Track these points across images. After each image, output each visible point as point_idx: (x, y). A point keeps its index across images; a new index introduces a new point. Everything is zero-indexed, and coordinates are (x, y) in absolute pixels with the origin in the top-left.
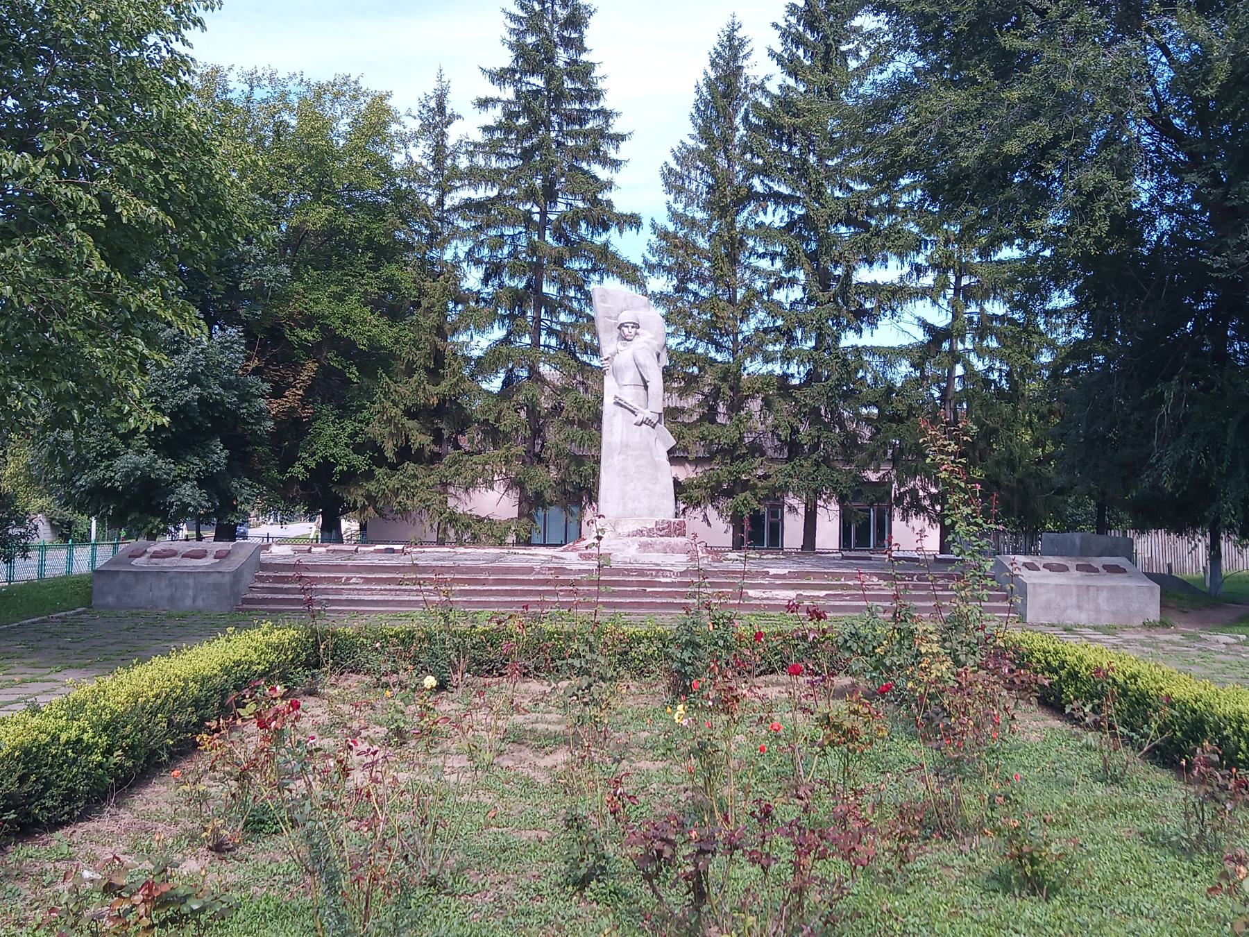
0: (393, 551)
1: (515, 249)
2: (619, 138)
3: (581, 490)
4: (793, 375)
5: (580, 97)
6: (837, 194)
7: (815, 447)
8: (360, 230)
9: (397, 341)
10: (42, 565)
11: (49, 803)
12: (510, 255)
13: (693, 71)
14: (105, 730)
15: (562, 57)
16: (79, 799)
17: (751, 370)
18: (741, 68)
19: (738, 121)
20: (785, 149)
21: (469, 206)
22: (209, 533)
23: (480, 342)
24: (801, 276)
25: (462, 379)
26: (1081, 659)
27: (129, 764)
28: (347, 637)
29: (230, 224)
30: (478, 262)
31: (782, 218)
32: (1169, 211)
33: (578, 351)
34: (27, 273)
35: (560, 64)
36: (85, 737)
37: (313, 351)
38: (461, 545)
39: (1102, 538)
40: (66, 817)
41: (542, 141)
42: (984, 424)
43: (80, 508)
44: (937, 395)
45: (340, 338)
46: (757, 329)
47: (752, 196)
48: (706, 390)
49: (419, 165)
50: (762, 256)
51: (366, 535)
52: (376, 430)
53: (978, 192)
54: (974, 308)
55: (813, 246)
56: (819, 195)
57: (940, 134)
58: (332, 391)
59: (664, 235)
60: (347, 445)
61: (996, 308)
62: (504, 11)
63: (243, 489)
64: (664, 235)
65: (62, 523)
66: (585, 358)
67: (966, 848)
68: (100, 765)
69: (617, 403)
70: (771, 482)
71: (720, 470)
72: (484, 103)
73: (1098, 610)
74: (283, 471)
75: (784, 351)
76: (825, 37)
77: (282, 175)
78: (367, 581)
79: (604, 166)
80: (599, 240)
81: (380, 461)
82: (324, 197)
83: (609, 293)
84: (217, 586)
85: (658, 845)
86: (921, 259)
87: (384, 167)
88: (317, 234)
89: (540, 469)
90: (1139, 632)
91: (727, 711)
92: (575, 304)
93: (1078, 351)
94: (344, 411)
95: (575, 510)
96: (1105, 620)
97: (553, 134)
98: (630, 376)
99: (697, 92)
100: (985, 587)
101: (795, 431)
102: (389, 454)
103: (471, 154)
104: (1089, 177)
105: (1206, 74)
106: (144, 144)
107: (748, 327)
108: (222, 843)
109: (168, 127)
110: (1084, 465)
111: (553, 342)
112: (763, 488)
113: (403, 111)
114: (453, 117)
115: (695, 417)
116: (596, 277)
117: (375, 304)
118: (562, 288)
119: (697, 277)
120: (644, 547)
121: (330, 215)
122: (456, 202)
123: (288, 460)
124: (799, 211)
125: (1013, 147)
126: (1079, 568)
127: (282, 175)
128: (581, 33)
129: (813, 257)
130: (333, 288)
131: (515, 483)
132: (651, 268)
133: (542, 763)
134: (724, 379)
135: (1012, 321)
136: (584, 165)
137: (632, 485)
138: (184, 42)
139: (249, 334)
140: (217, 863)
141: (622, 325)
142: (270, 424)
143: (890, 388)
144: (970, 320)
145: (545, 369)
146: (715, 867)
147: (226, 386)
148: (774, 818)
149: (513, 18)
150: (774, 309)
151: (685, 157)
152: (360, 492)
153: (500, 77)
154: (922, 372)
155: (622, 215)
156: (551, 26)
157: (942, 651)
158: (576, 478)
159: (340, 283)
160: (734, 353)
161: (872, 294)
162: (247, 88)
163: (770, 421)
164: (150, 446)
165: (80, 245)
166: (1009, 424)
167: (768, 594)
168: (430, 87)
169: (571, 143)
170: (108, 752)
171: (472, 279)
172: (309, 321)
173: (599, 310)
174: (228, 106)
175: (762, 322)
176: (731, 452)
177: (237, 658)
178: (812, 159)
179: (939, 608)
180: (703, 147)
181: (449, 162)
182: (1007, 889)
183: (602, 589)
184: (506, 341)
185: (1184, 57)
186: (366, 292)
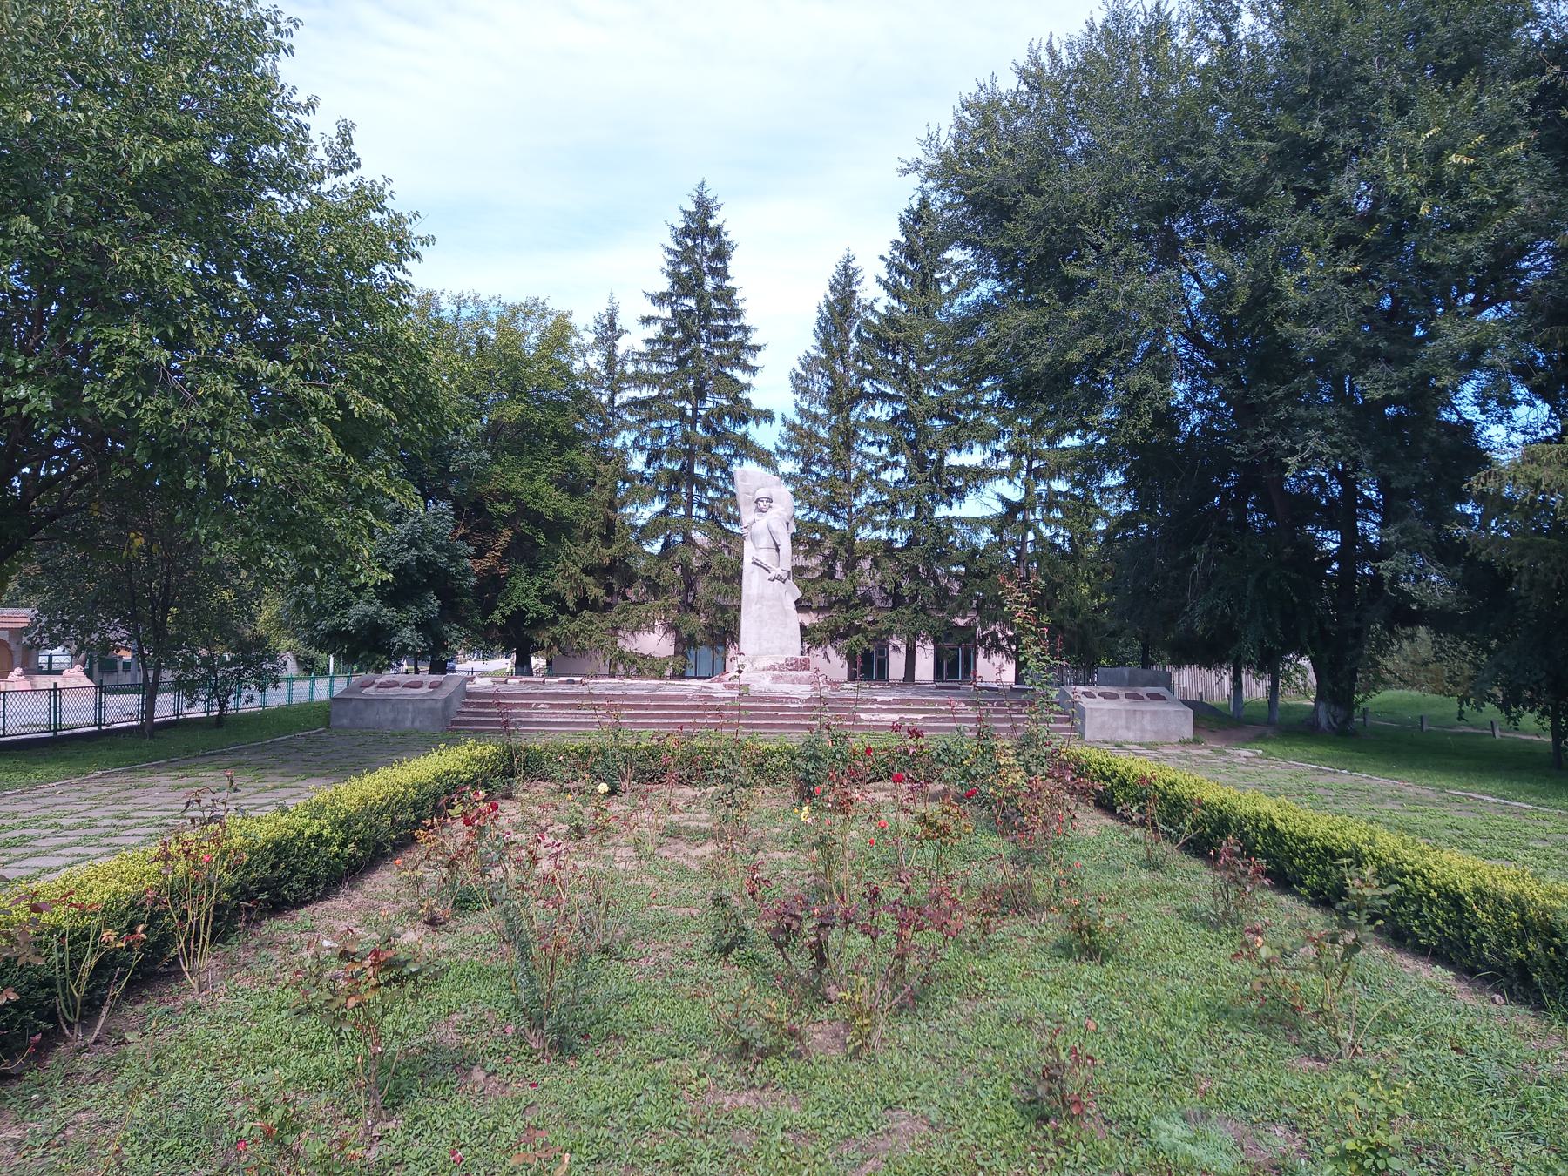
2: (756, 348)
3: (725, 634)
5: (725, 315)
6: (932, 393)
10: (290, 694)
11: (296, 886)
12: (668, 443)
13: (816, 294)
15: (710, 283)
19: (852, 335)
21: (634, 403)
23: (643, 514)
24: (903, 460)
25: (629, 544)
26: (1129, 770)
27: (360, 854)
30: (642, 449)
32: (1200, 407)
33: (723, 521)
35: (709, 289)
37: (509, 520)
39: (1146, 672)
41: (694, 351)
43: (321, 647)
45: (531, 510)
47: (863, 395)
49: (595, 371)
50: (872, 444)
51: (551, 669)
52: (559, 584)
53: (1046, 393)
54: (1042, 486)
55: (913, 436)
57: (1015, 345)
58: (524, 553)
59: (792, 427)
61: (1060, 486)
63: (452, 632)
64: (792, 427)
65: (306, 660)
66: (728, 526)
67: (1036, 922)
68: (337, 855)
70: (878, 626)
71: (838, 617)
72: (647, 321)
73: (1143, 730)
74: (484, 618)
76: (922, 267)
80: (740, 431)
81: (563, 609)
83: (747, 472)
84: (431, 711)
88: (512, 426)
89: (692, 615)
91: (843, 812)
93: (1126, 521)
94: (534, 569)
95: (721, 649)
96: (1148, 738)
98: (765, 541)
100: (1051, 711)
101: (898, 585)
102: (570, 604)
103: (637, 362)
104: (1136, 380)
106: (372, 354)
107: (861, 502)
110: (1121, 619)
111: (703, 513)
113: (581, 327)
114: (622, 332)
115: (818, 574)
116: (738, 461)
117: (560, 483)
118: (710, 470)
120: (776, 679)
122: (625, 400)
123: (489, 609)
124: (901, 408)
125: (1074, 356)
126: (1127, 696)
130: (525, 470)
131: (672, 628)
132: (782, 453)
133: (693, 854)
134: (841, 543)
135: (1073, 497)
136: (728, 371)
138: (405, 271)
139: (457, 507)
140: (431, 934)
142: (474, 580)
143: (975, 551)
144: (1040, 495)
145: (696, 535)
147: (438, 549)
149: (670, 251)
150: (881, 487)
151: (809, 364)
153: (660, 299)
158: (721, 624)
159: (530, 465)
160: (849, 522)
161: (961, 475)
162: (455, 309)
163: (877, 577)
165: (320, 435)
168: (603, 307)
169: (717, 353)
170: (343, 844)
171: (638, 462)
172: (506, 497)
173: (740, 488)
174: (440, 323)
176: (846, 603)
179: (1014, 728)
180: (824, 356)
182: (1070, 955)
184: (664, 512)
185: (1212, 283)
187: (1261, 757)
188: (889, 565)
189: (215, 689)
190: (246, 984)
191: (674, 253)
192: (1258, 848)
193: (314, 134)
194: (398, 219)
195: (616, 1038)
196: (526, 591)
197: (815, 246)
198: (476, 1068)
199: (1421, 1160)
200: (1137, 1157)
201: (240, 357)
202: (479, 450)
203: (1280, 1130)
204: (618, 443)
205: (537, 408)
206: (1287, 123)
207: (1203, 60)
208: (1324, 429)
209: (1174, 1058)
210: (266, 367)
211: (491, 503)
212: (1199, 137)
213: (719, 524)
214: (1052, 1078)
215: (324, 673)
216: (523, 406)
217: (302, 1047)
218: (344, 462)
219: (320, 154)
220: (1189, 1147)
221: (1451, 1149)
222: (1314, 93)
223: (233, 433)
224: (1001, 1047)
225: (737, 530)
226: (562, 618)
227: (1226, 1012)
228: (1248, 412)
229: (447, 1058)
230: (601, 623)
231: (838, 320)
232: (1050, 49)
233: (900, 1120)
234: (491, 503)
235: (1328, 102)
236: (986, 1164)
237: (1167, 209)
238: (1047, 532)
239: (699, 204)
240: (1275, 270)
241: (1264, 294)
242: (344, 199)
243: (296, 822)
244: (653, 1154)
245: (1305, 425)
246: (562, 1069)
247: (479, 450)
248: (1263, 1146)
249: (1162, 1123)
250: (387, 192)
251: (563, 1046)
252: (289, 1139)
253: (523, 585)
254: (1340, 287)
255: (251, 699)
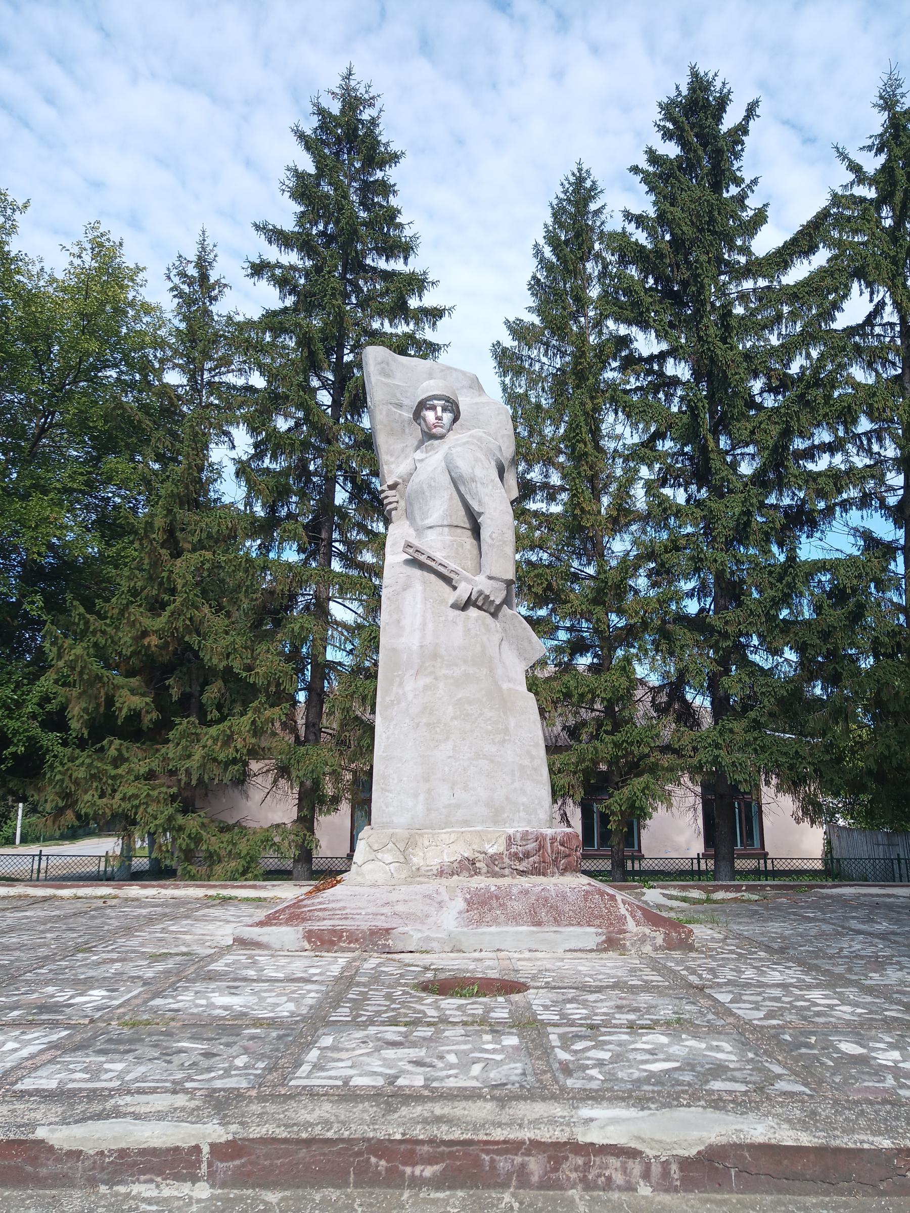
60: (34, 716)
69: (414, 562)
98: (441, 507)
99: (536, 255)
120: (481, 906)
141: (423, 405)
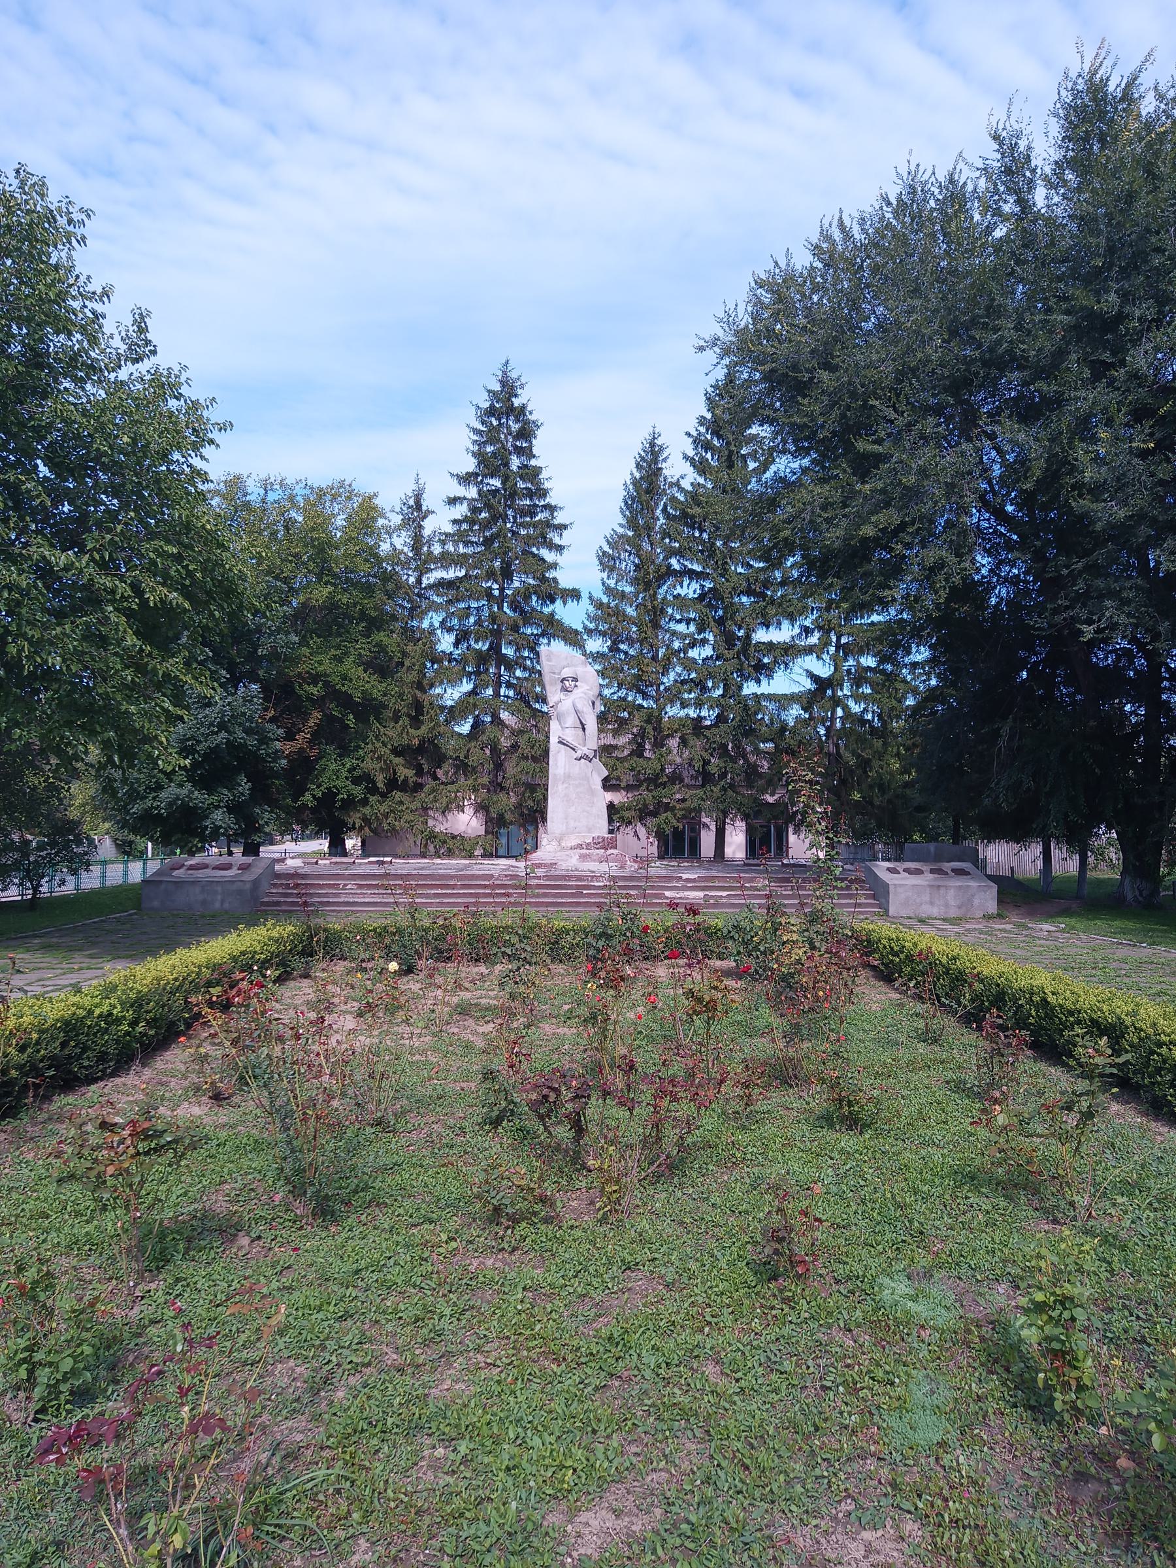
0: (383, 863)
1: (480, 619)
2: (562, 527)
3: (533, 815)
4: (705, 718)
5: (530, 494)
6: (740, 570)
7: (723, 775)
8: (355, 605)
9: (385, 695)
10: (103, 876)
11: (86, 1063)
12: (475, 623)
13: (622, 472)
14: (132, 1006)
15: (515, 462)
16: (111, 1060)
17: (670, 714)
18: (661, 469)
19: (658, 512)
20: (697, 534)
21: (442, 584)
22: (238, 850)
23: (452, 694)
24: (711, 638)
25: (438, 724)
26: (915, 945)
27: (152, 1032)
28: (336, 932)
29: (242, 603)
30: (450, 630)
31: (695, 591)
32: (1005, 580)
33: (531, 702)
34: (74, 646)
35: (514, 468)
36: (115, 1012)
37: (318, 703)
38: (439, 857)
39: (956, 847)
40: (100, 1074)
41: (500, 530)
42: (860, 755)
43: (134, 830)
44: (822, 732)
45: (339, 691)
46: (676, 681)
47: (670, 572)
48: (635, 730)
49: (402, 552)
50: (679, 621)
51: (367, 849)
52: (369, 765)
53: (847, 571)
54: (851, 662)
55: (721, 612)
56: (725, 572)
57: (811, 521)
58: (335, 735)
59: (599, 605)
61: (869, 661)
62: (468, 426)
63: (265, 816)
64: (599, 605)
65: (124, 842)
66: (537, 706)
67: (804, 1094)
68: (128, 1033)
69: (560, 742)
70: (688, 803)
71: (646, 795)
72: (453, 501)
73: (947, 905)
74: (295, 800)
75: (697, 698)
76: (728, 443)
77: (291, 562)
78: (360, 886)
79: (550, 550)
80: (547, 610)
81: (374, 790)
82: (325, 579)
83: (555, 655)
84: (240, 892)
85: (545, 1091)
86: (808, 623)
87: (374, 556)
88: (321, 608)
89: (502, 795)
90: (980, 923)
91: (615, 988)
92: (528, 662)
93: (932, 696)
94: (345, 751)
95: (531, 828)
96: (953, 913)
97: (509, 525)
98: (571, 720)
100: (835, 887)
101: (706, 763)
102: (380, 785)
103: (443, 543)
104: (931, 555)
105: (1026, 472)
106: (168, 542)
107: (669, 679)
108: (219, 1093)
109: (187, 526)
110: (922, 791)
111: (511, 693)
112: (681, 809)
113: (387, 509)
114: (429, 512)
115: (626, 752)
116: (545, 641)
117: (368, 666)
118: (518, 650)
119: (627, 639)
120: (583, 858)
121: (330, 593)
122: (432, 581)
123: (300, 791)
124: (708, 585)
125: (868, 531)
126: (932, 871)
127: (291, 562)
128: (531, 442)
129: (720, 622)
130: (333, 652)
131: (481, 807)
132: (590, 632)
133: (481, 1030)
134: (648, 721)
135: (883, 672)
136: (534, 550)
137: (573, 808)
138: (202, 457)
139: (266, 690)
140: (216, 1109)
142: (284, 762)
143: (784, 728)
144: (849, 671)
145: (504, 715)
146: (594, 1108)
147: (248, 731)
148: (637, 1070)
149: (476, 431)
150: (689, 664)
151: (616, 542)
152: (358, 815)
153: (466, 479)
154: (810, 714)
155: (565, 590)
156: (506, 437)
157: (800, 939)
158: (530, 803)
159: (338, 647)
160: (656, 701)
161: (769, 651)
162: (262, 492)
163: (686, 754)
164: (188, 781)
165: (117, 624)
166: (880, 755)
167: (681, 894)
168: (409, 489)
169: (523, 532)
170: (134, 1023)
171: (446, 642)
172: (314, 679)
173: (546, 666)
174: (247, 505)
175: (680, 675)
176: (654, 781)
177: (243, 949)
178: (719, 543)
179: (802, 905)
180: (630, 534)
181: (425, 549)
182: (831, 1126)
183: (529, 891)
184: (473, 692)
185: (1010, 457)
186: (360, 654)
187: (1063, 931)
188: (698, 743)
189: (28, 871)
190: (30, 1156)
191: (479, 432)
192: (1032, 1020)
193: (109, 326)
194: (195, 405)
195: (378, 1205)
196: (336, 773)
197: (619, 425)
198: (241, 1234)
199: (1131, 1315)
200: (858, 1313)
201: (34, 548)
202: (287, 633)
203: (1002, 1288)
204: (425, 624)
205: (345, 590)
206: (1083, 298)
207: (999, 233)
208: (1121, 600)
209: (911, 1222)
210: (60, 559)
211: (300, 685)
212: (993, 311)
213: (528, 704)
214: (781, 1240)
215: (142, 855)
216: (330, 588)
217: (78, 1214)
218: (142, 650)
219: (117, 343)
220: (910, 1304)
221: (1160, 1302)
222: (1109, 266)
223: (28, 622)
224: (747, 1212)
225: (545, 709)
226: (372, 799)
227: (973, 1179)
228: (1052, 585)
229: (213, 1224)
230: (411, 803)
231: (645, 497)
232: (841, 224)
233: (637, 1281)
234: (300, 685)
235: (1124, 273)
236: (715, 1320)
237: (959, 385)
238: (856, 708)
239: (504, 383)
240: (1070, 443)
241: (1060, 466)
242: (140, 387)
243: (87, 1002)
244: (396, 1311)
245: (1101, 597)
246: (324, 1235)
247: (287, 633)
248: (982, 1302)
249: (887, 1281)
250: (183, 380)
251: (326, 1211)
252: (42, 1296)
253: (333, 766)
254: (1135, 461)
255: (63, 882)
